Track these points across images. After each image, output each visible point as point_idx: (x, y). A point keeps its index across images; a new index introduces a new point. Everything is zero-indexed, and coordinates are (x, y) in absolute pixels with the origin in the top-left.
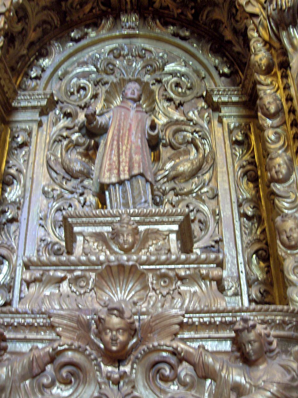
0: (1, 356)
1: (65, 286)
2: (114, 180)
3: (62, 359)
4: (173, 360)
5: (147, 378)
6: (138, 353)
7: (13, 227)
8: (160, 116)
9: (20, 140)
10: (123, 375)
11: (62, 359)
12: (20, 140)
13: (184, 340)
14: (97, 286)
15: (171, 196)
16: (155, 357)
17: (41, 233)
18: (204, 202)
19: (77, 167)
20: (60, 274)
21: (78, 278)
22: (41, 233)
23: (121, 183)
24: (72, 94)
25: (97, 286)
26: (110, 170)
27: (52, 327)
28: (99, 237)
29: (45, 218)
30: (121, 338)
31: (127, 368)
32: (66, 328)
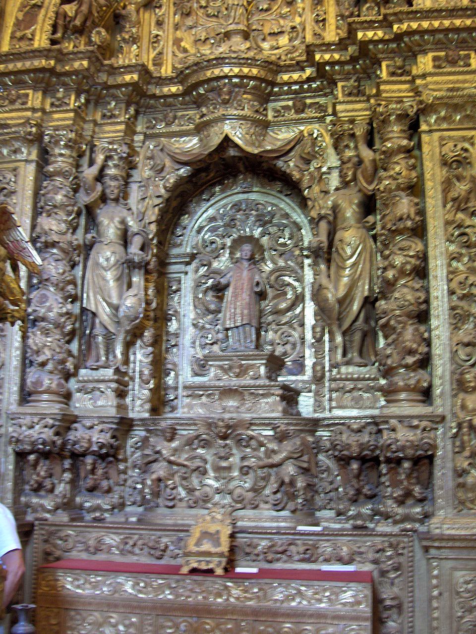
0: (475, 586)
1: (204, 398)
2: (232, 326)
3: (201, 438)
4: (112, 451)
5: (237, 446)
6: (231, 436)
7: (175, 350)
8: (269, 263)
9: (174, 288)
10: (226, 445)
11: (201, 438)
12: (174, 288)
13: (253, 430)
14: (220, 399)
15: (274, 326)
16: (239, 438)
17: (192, 352)
18: (294, 329)
19: (212, 307)
20: (201, 393)
21: (210, 394)
22: (192, 352)
23: (237, 327)
24: (207, 246)
25: (220, 399)
26: (230, 319)
27: (195, 424)
28: (221, 367)
29: (194, 343)
30: (224, 430)
31: (228, 442)
32: (203, 425)
